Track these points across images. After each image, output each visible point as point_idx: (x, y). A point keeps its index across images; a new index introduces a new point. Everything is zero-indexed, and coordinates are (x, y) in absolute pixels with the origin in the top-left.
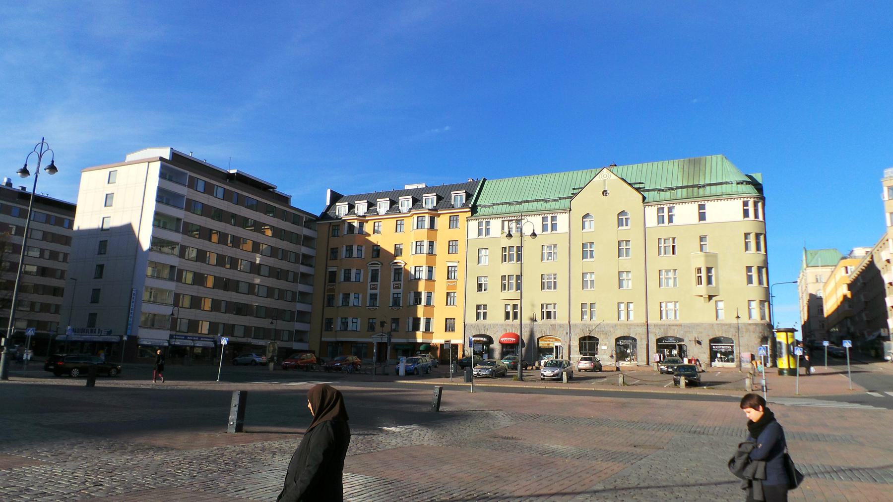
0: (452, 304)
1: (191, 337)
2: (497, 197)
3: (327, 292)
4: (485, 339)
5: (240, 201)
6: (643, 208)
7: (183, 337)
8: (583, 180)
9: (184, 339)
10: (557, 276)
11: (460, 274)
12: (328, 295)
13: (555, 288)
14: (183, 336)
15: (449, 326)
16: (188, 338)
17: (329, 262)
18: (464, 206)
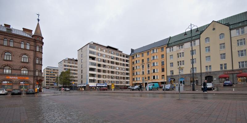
11: (165, 63)
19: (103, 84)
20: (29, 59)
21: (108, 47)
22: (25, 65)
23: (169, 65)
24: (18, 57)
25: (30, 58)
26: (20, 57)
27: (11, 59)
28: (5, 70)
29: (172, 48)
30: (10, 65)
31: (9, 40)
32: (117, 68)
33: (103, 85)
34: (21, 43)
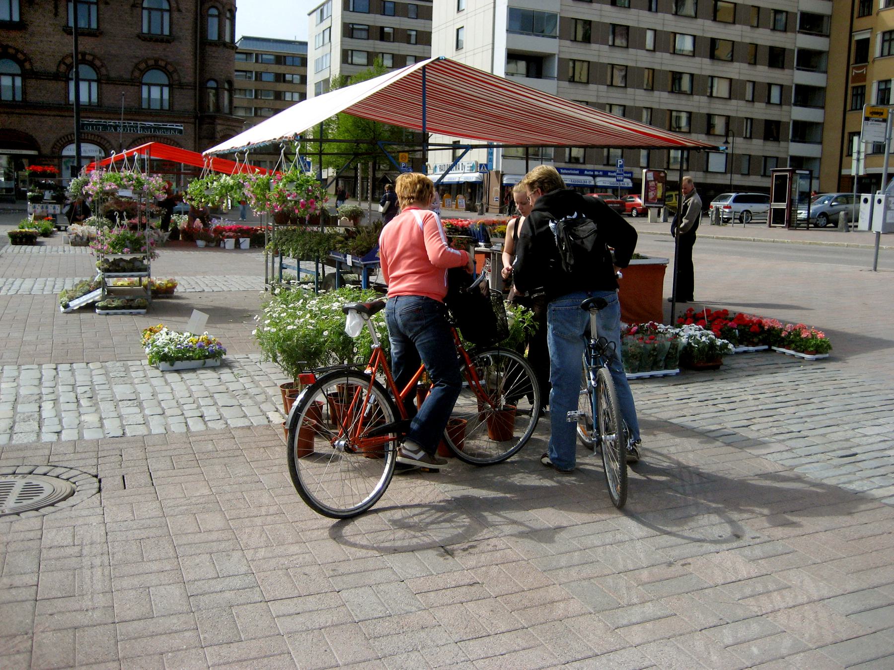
1: (591, 171)
3: (853, 82)
7: (578, 172)
9: (585, 170)
12: (853, 88)
14: (576, 170)
16: (586, 172)
17: (856, 21)
19: (605, 174)
20: (176, 15)
22: (159, 51)
25: (179, 10)
27: (94, 25)
28: (145, 89)
30: (95, 57)
32: (721, 88)
33: (601, 181)
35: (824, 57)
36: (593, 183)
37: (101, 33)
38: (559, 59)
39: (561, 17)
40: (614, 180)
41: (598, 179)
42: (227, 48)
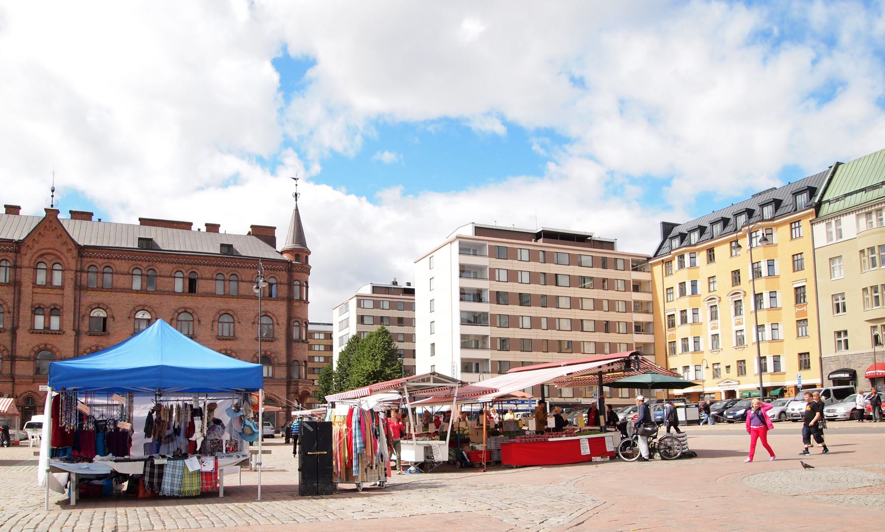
0: (804, 334)
2: (872, 177)
4: (847, 375)
5: (548, 258)
6: (810, 226)
8: (710, 219)
10: (846, 296)
13: (844, 310)
15: (804, 362)
18: (808, 207)
21: (583, 522)
23: (827, 305)
24: (250, 324)
26: (253, 323)
29: (838, 223)
31: (101, 269)
34: (175, 277)
35: (651, 325)
36: (516, 408)
37: (236, 339)
38: (491, 338)
39: (490, 314)
40: (528, 405)
41: (519, 406)
42: (304, 343)
